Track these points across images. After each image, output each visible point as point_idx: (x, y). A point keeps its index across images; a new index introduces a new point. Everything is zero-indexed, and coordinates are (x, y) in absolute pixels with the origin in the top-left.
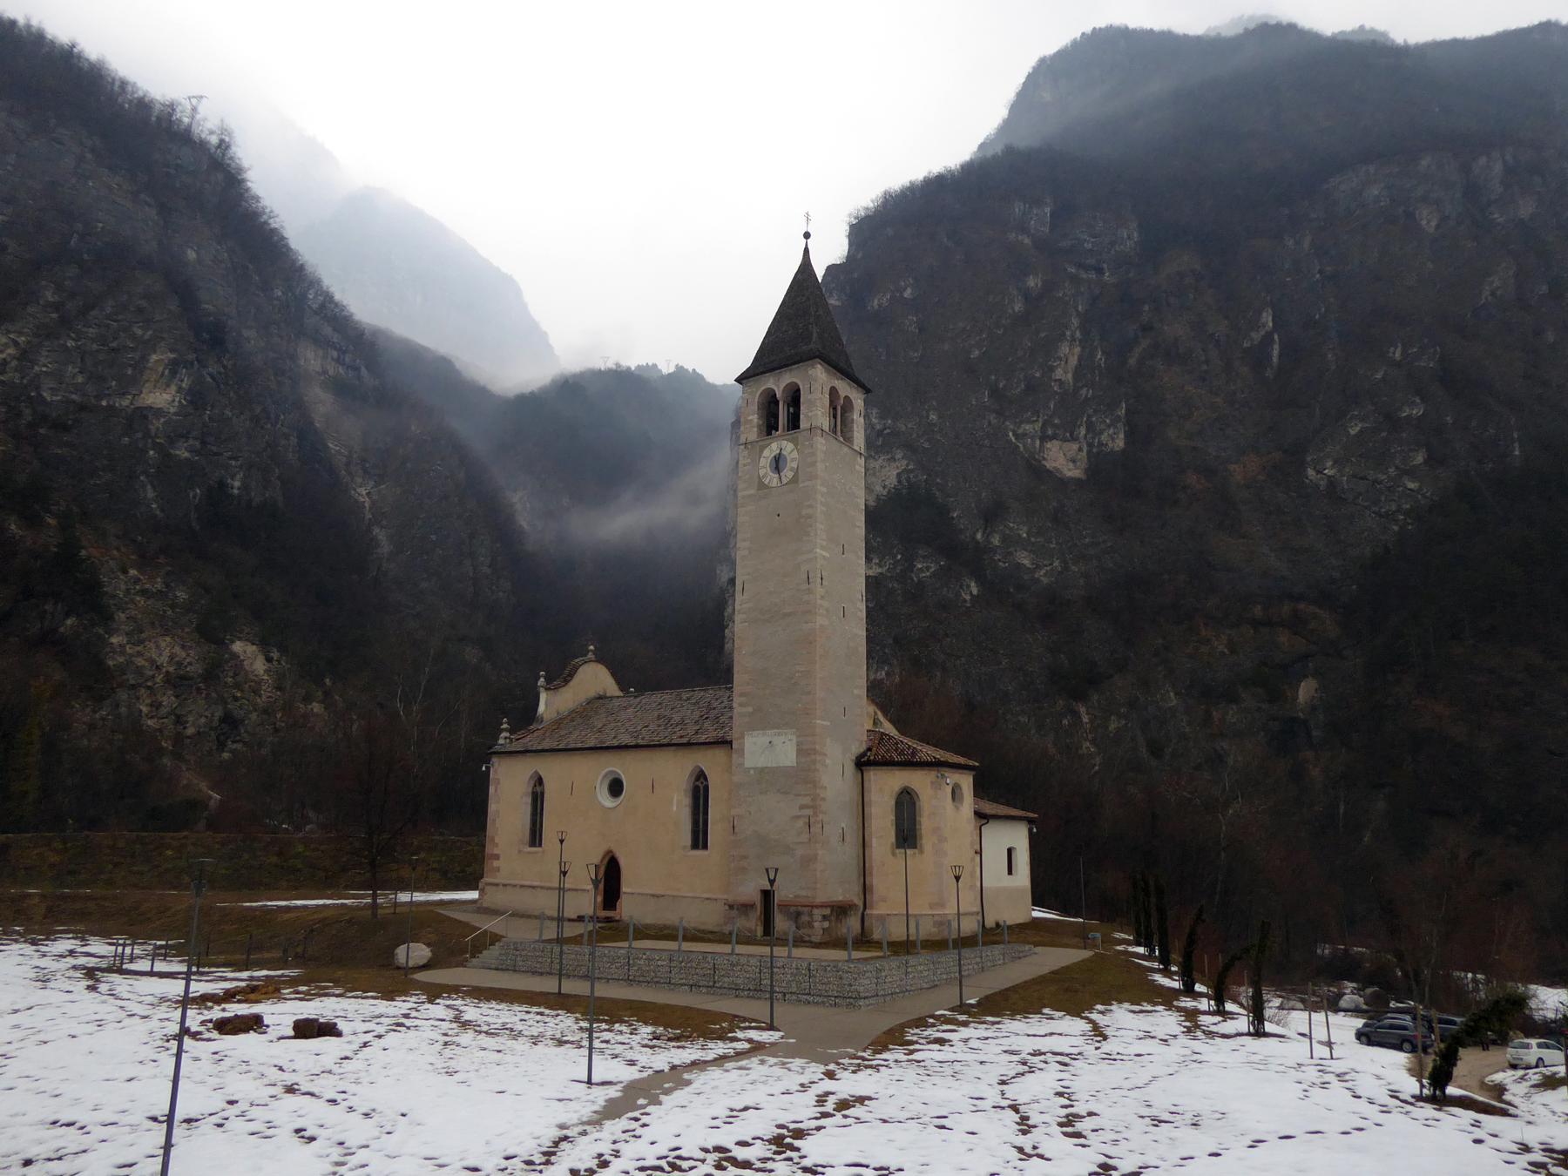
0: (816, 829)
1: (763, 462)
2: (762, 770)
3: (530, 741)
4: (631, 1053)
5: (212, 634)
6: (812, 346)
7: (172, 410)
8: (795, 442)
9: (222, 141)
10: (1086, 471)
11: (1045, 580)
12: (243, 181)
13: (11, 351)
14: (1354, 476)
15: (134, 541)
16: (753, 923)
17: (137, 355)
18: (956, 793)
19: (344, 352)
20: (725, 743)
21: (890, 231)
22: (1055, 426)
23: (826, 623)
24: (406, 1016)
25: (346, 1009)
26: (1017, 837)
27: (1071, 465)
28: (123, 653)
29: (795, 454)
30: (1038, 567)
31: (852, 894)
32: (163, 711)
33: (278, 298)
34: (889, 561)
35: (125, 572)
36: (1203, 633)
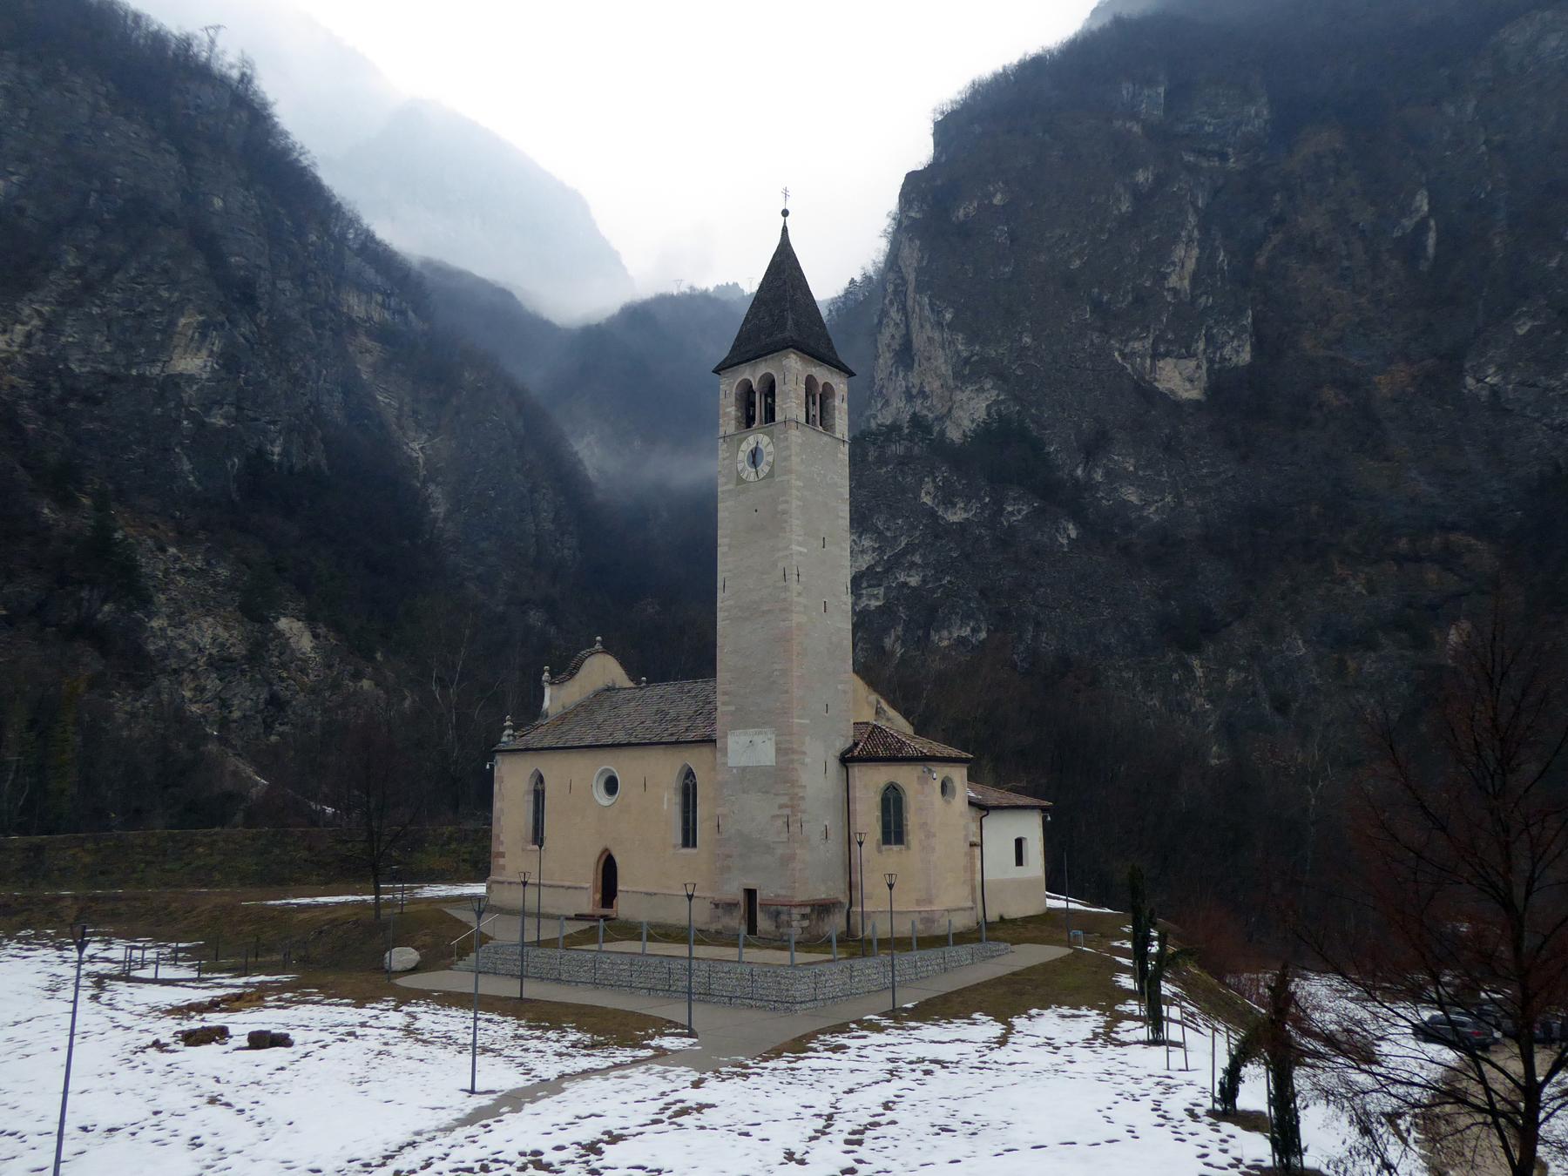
1: (741, 455)
2: (744, 769)
3: (533, 738)
4: (548, 1055)
6: (787, 334)
7: (205, 376)
9: (243, 75)
11: (1156, 518)
12: (270, 117)
13: (36, 322)
14: (1522, 384)
15: (173, 517)
16: (737, 922)
17: (165, 319)
18: (945, 787)
19: (389, 296)
20: (710, 741)
21: (977, 129)
22: (1169, 342)
24: (363, 1025)
25: (306, 1019)
26: (1031, 828)
27: (1188, 386)
28: (165, 637)
29: (771, 448)
30: (1147, 504)
31: (837, 891)
32: (208, 695)
33: (312, 244)
34: (975, 505)
35: (163, 550)
36: (1338, 571)
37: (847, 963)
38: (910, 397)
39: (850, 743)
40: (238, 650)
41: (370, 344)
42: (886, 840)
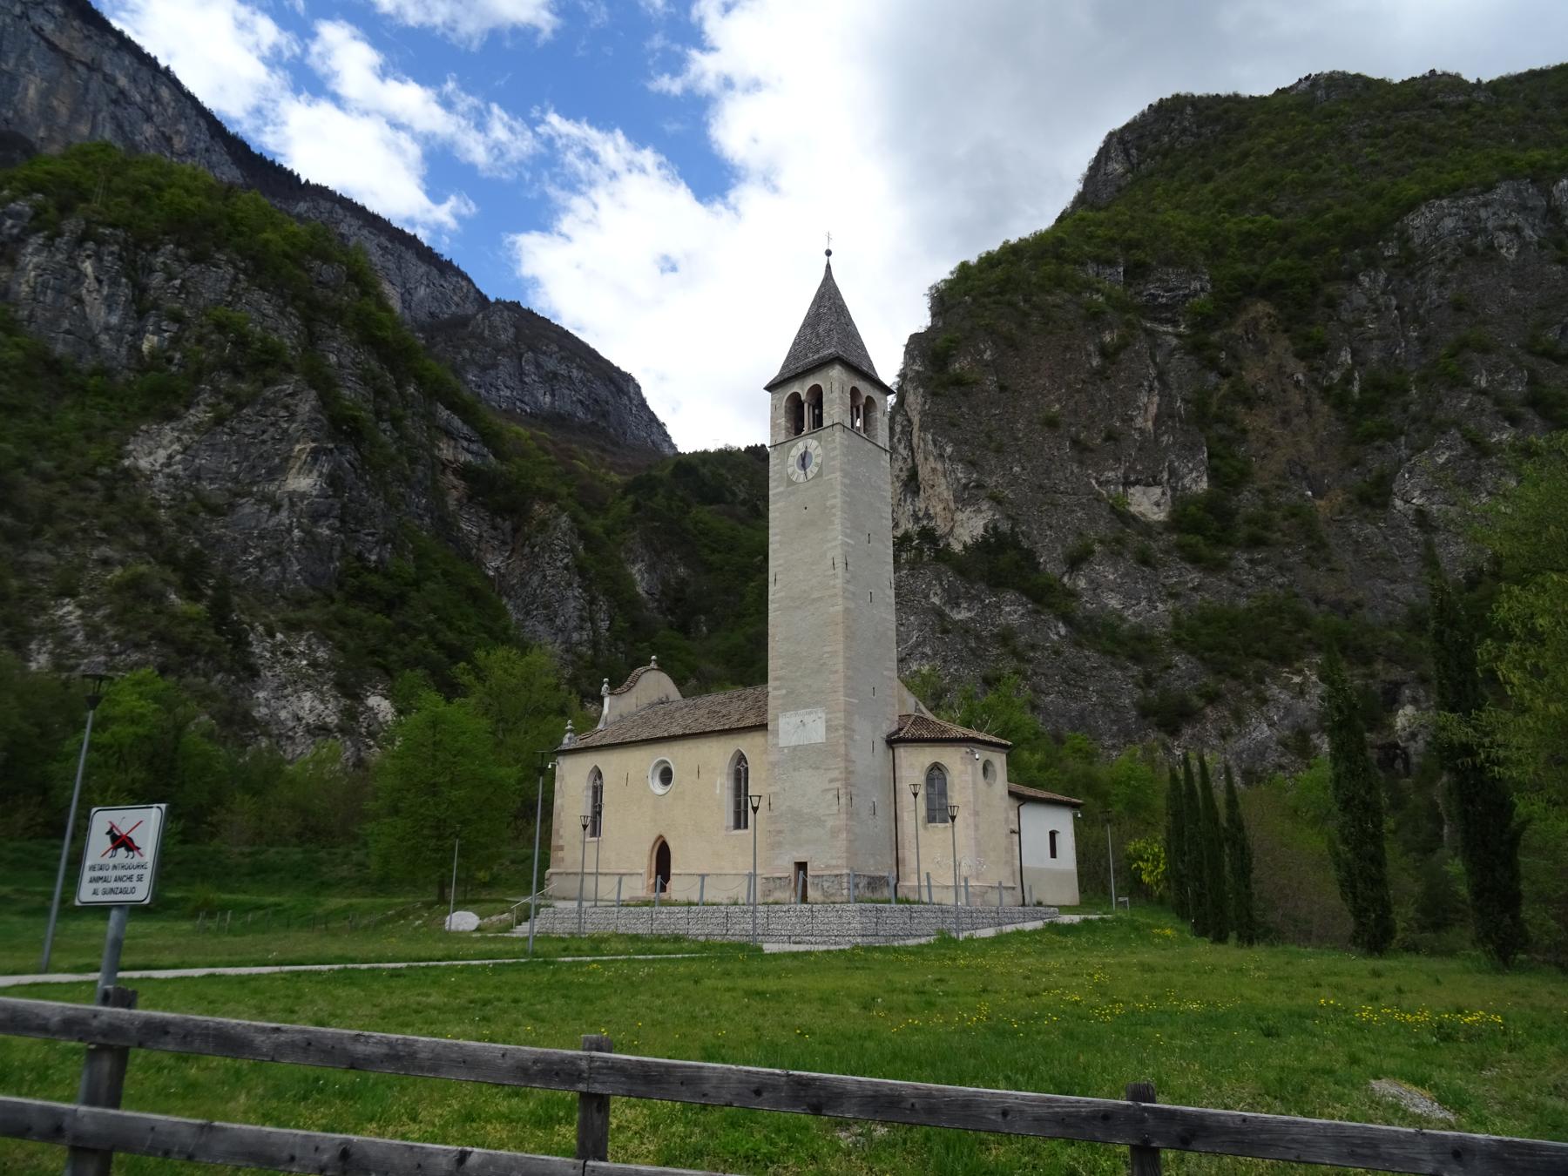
2: (795, 748)
5: (351, 691)
8: (819, 440)
10: (1170, 515)
18: (986, 768)
20: (763, 727)
27: (1156, 509)
29: (819, 451)
31: (887, 871)
35: (273, 636)
38: (917, 519)
39: (895, 727)
40: (332, 720)
41: (456, 482)
42: (931, 819)
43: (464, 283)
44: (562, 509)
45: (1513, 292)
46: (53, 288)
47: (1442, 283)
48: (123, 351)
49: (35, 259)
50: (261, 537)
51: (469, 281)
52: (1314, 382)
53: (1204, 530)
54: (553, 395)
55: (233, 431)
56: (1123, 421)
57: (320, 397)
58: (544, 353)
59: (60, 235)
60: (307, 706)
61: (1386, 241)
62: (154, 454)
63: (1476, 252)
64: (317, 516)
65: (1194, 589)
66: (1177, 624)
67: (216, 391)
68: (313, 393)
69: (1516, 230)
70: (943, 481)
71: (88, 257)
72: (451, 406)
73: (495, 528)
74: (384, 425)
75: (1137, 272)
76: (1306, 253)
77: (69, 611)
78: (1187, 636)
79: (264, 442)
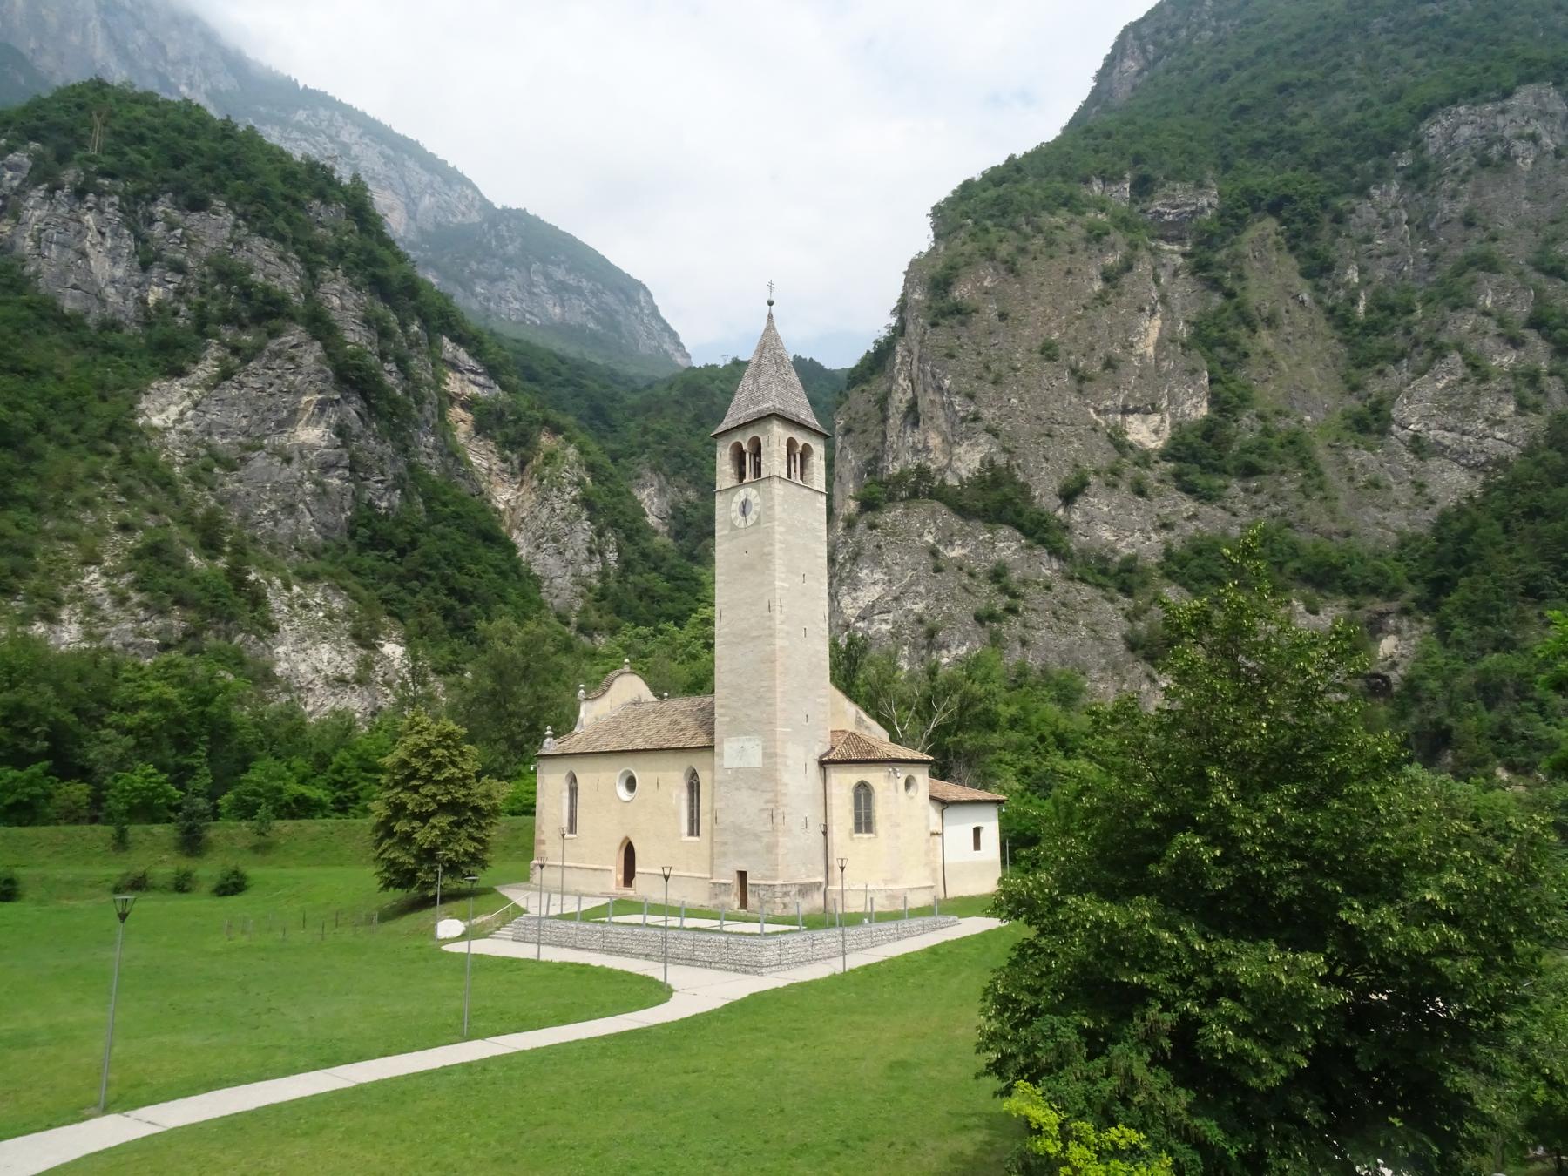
0: (779, 819)
2: (737, 770)
5: (365, 639)
18: (908, 783)
23: (787, 644)
27: (1154, 437)
29: (758, 500)
37: (809, 934)
39: (828, 748)
40: (350, 671)
42: (858, 829)
43: (469, 192)
44: (569, 440)
45: (1526, 206)
46: (57, 243)
47: (1454, 196)
48: (130, 304)
49: (37, 213)
50: (274, 490)
51: (475, 189)
52: (1319, 302)
53: (1199, 458)
54: (563, 306)
55: (242, 385)
56: (1124, 347)
57: (325, 347)
58: (552, 263)
59: (61, 188)
60: (325, 658)
61: (1400, 151)
62: (166, 410)
63: (1492, 161)
64: (327, 468)
65: (1189, 518)
66: (1168, 554)
67: (223, 344)
68: (318, 344)
69: (1534, 138)
70: (941, 413)
71: (90, 209)
72: (458, 340)
73: (504, 460)
74: (388, 367)
75: (1143, 187)
76: (1317, 165)
77: (94, 579)
78: (1176, 566)
79: (271, 395)
